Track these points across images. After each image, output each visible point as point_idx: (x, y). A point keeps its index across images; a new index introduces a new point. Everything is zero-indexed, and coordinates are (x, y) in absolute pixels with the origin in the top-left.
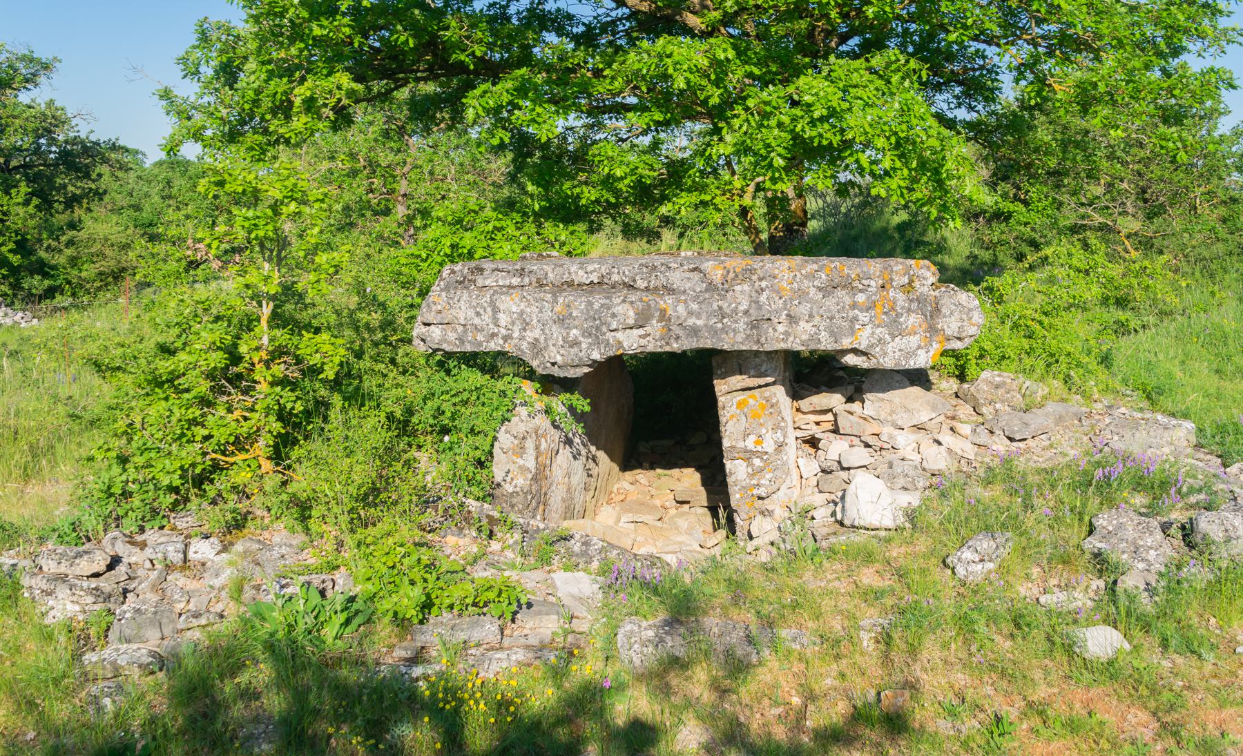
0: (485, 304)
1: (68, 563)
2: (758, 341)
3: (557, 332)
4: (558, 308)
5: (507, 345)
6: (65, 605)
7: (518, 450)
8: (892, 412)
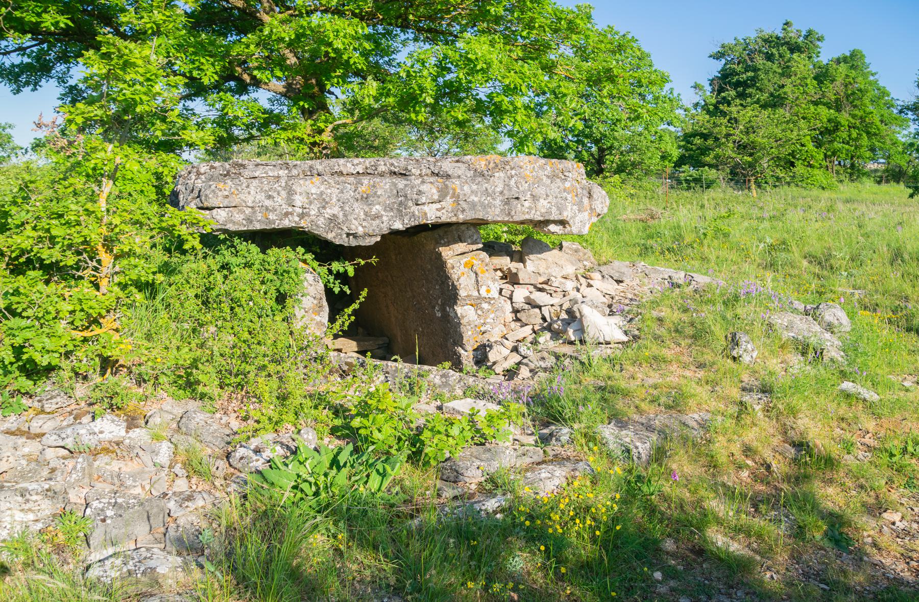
0: (279, 188)
2: (509, 214)
3: (359, 209)
4: (362, 189)
5: (302, 221)
6: (12, 516)
7: (317, 309)
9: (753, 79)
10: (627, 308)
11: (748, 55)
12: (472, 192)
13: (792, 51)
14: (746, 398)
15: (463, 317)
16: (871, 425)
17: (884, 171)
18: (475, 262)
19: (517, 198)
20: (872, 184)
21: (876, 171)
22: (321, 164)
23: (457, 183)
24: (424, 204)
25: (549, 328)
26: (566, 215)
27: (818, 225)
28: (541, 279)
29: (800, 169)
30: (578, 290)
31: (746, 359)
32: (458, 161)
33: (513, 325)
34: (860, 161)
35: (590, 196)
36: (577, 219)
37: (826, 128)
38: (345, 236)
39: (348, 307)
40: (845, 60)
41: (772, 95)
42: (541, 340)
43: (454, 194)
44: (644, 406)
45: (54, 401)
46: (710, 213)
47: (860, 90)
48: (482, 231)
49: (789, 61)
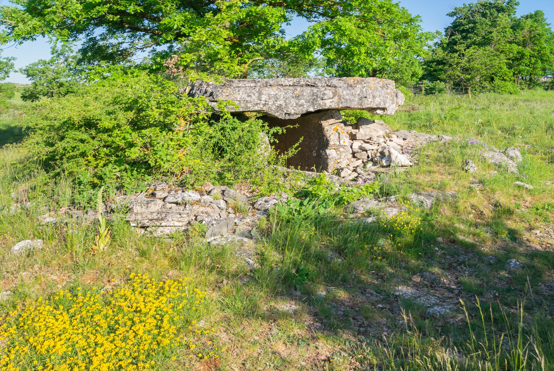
1: (145, 207)
3: (293, 102)
8: (370, 132)
9: (473, 29)
10: (410, 151)
11: (471, 13)
13: (499, 11)
14: (472, 185)
16: (529, 199)
17: (551, 83)
18: (338, 128)
19: (366, 97)
20: (542, 90)
21: (545, 82)
22: (272, 80)
25: (372, 160)
26: (387, 105)
27: (507, 113)
29: (497, 81)
30: (385, 143)
31: (471, 170)
33: (352, 159)
34: (536, 77)
37: (516, 57)
39: (294, 145)
40: (531, 16)
41: (483, 38)
44: (426, 188)
45: (161, 185)
46: (446, 108)
47: (539, 35)
49: (496, 18)
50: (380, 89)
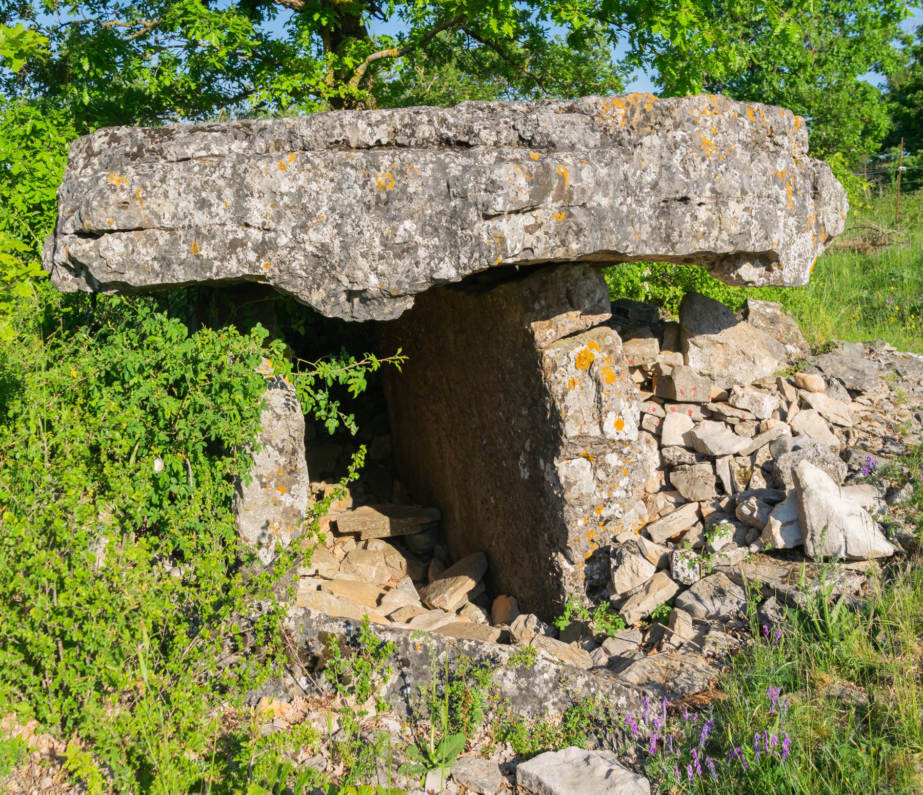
0: (221, 183)
4: (379, 179)
5: (263, 262)
7: (286, 477)
8: (727, 363)
10: (881, 463)
12: (598, 184)
15: (570, 485)
19: (685, 200)
23: (569, 161)
24: (499, 215)
25: (731, 512)
26: (778, 238)
28: (717, 390)
30: (784, 417)
32: (570, 110)
35: (816, 195)
36: (794, 250)
38: (343, 297)
42: (716, 543)
43: (561, 188)
48: (606, 278)
50: (742, 155)
